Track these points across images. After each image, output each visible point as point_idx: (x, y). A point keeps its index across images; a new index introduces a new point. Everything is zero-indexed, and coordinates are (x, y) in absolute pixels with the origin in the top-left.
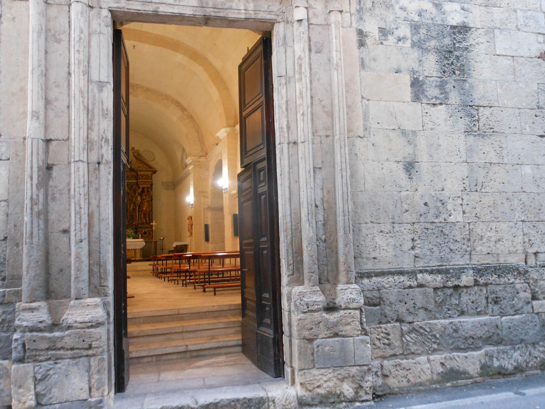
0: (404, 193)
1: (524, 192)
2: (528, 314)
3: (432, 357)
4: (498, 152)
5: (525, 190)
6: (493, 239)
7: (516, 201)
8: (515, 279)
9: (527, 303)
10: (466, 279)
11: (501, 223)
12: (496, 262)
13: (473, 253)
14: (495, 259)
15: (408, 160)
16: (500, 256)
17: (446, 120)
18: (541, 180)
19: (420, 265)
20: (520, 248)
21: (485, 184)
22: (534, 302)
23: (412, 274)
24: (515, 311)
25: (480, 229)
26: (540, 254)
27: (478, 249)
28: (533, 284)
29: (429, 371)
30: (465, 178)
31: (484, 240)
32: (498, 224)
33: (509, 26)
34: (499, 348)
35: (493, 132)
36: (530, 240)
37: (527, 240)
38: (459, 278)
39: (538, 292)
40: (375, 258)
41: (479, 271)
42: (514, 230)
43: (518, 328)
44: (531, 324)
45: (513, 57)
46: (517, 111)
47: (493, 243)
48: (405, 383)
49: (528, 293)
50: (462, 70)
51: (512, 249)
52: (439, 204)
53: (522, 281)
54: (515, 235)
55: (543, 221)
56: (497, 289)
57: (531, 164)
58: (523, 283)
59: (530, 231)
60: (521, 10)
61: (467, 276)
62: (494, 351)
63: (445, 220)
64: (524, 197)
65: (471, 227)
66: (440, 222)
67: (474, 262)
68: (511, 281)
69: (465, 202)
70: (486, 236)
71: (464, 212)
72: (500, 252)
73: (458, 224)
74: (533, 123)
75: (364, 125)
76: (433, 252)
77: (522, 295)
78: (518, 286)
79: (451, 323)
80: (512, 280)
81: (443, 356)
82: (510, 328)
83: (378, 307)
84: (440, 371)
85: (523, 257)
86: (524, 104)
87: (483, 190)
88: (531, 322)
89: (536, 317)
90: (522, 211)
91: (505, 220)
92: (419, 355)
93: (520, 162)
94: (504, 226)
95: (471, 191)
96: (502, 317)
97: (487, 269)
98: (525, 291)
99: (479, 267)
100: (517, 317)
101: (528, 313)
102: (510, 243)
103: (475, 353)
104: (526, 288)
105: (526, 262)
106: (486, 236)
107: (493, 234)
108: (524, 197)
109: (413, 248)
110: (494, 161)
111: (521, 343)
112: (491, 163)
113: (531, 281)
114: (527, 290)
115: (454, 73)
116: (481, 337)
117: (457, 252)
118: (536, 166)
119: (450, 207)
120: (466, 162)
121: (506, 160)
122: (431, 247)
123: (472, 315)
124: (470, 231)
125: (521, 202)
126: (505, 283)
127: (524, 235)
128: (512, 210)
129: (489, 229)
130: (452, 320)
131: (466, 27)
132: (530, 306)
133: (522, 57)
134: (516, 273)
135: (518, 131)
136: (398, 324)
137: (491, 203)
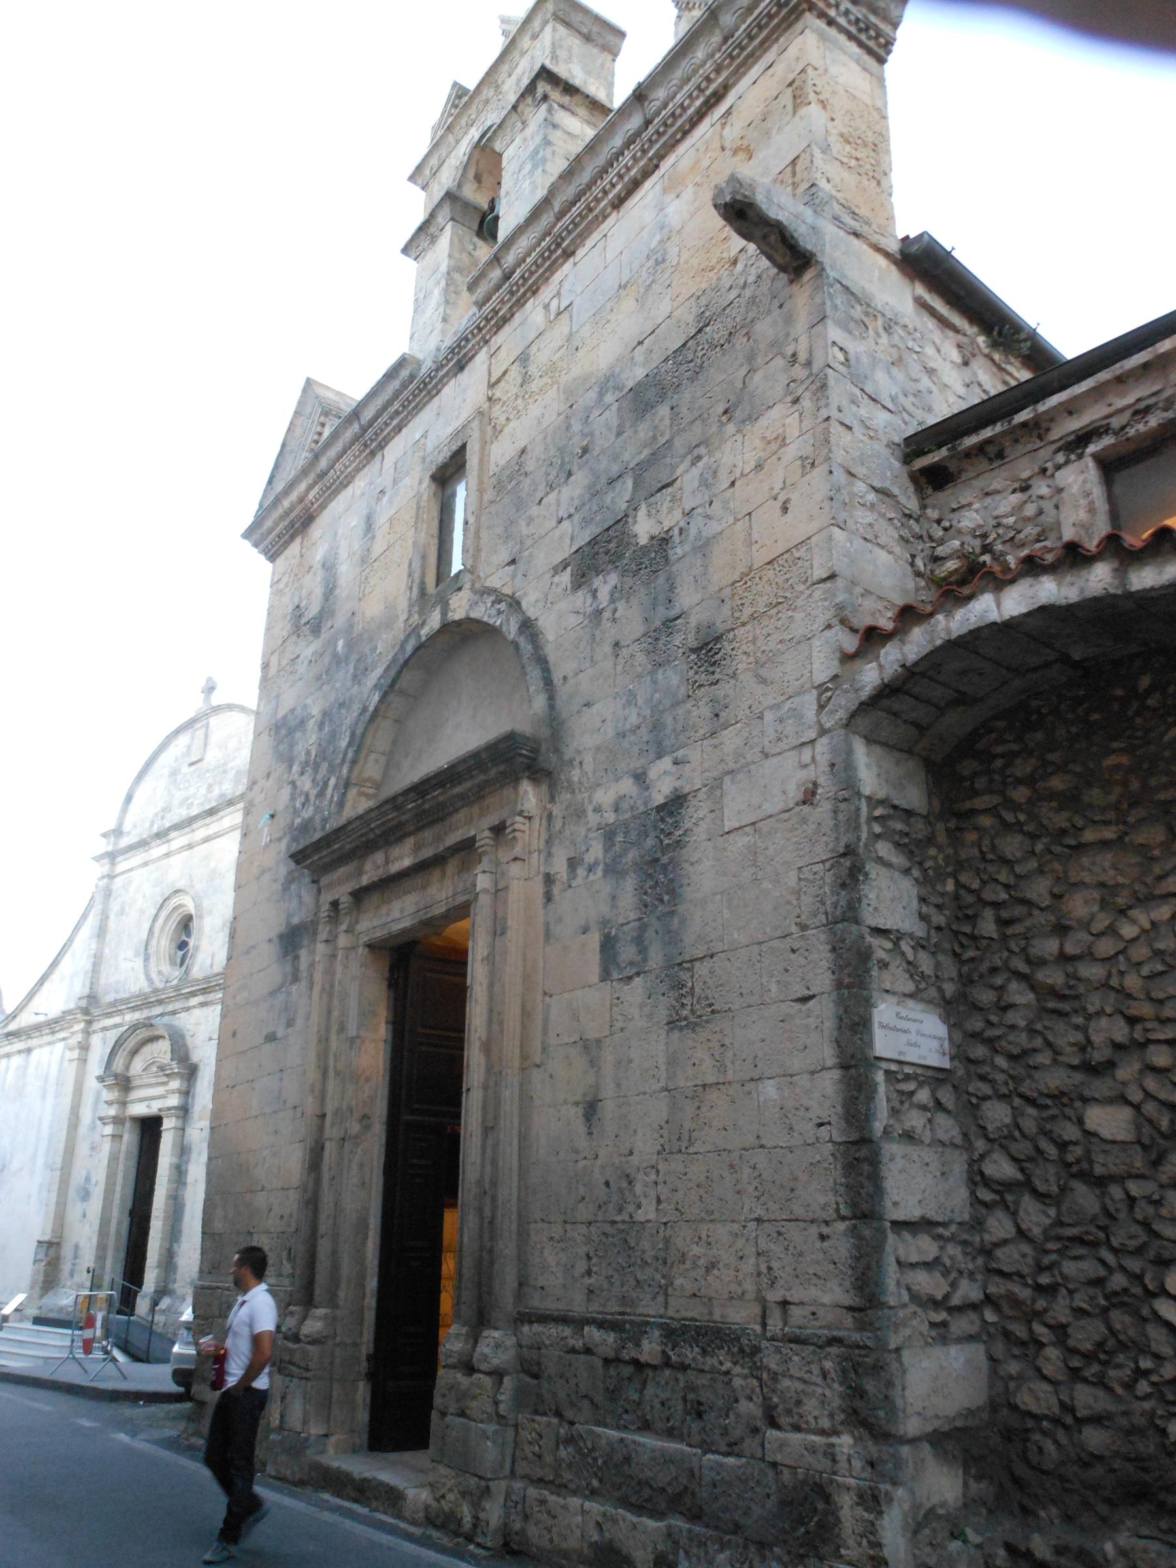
0: (581, 1164)
1: (762, 1146)
2: (752, 1461)
3: (587, 1505)
4: (717, 1057)
5: (763, 1142)
6: (702, 1262)
7: (746, 1172)
8: (735, 1364)
9: (752, 1431)
10: (650, 1348)
11: (718, 1225)
12: (707, 1318)
13: (670, 1291)
14: (706, 1311)
15: (588, 1099)
16: (715, 1302)
17: (642, 1006)
18: (798, 1113)
19: (594, 1309)
20: (749, 1286)
21: (695, 1134)
22: (772, 1434)
23: (578, 1324)
24: (730, 1445)
25: (682, 1238)
26: (792, 1307)
27: (678, 1282)
28: (769, 1383)
29: (578, 1532)
30: (663, 1124)
31: (688, 1264)
32: (711, 1226)
33: (749, 757)
34: (693, 1527)
35: (713, 1012)
36: (770, 1268)
37: (763, 1268)
38: (638, 1345)
39: (776, 1406)
40: (542, 1288)
41: (673, 1334)
42: (740, 1242)
43: (730, 1492)
44: (758, 1489)
45: (753, 824)
46: (756, 948)
47: (702, 1271)
48: (544, 1543)
49: (755, 1404)
50: (672, 892)
51: (734, 1287)
52: (624, 1184)
53: (746, 1371)
54: (740, 1254)
55: (796, 1220)
56: (699, 1382)
57: (778, 1076)
58: (746, 1377)
59: (772, 1246)
60: (771, 708)
61: (650, 1343)
62: (681, 1531)
63: (631, 1217)
64: (760, 1157)
65: (669, 1232)
66: (624, 1222)
67: (671, 1313)
68: (724, 1368)
69: (661, 1179)
70: (691, 1253)
71: (659, 1201)
72: (713, 1294)
73: (650, 1225)
74: (787, 971)
75: (542, 1043)
76: (612, 1284)
77: (744, 1407)
78: (737, 1382)
79: (622, 1440)
80: (728, 1365)
81: (602, 1509)
82: (715, 1486)
83: (535, 1382)
84: (593, 1540)
85: (757, 1310)
86: (768, 930)
87: (691, 1150)
88: (758, 1483)
89: (771, 1474)
90: (756, 1193)
91: (724, 1218)
92: (574, 1493)
93: (755, 1074)
94: (721, 1232)
95: (671, 1153)
96: (705, 1453)
97: (684, 1330)
98: (751, 1399)
99: (675, 1325)
100: (731, 1460)
101: (753, 1457)
102: (732, 1273)
103: (651, 1524)
104: (753, 1391)
105: (764, 1325)
106: (691, 1253)
107: (703, 1251)
108: (760, 1157)
109: (589, 1273)
110: (711, 1079)
111: (735, 1533)
112: (704, 1086)
113: (765, 1376)
114: (755, 1398)
115: (662, 901)
116: (663, 1490)
117: (646, 1288)
118: (788, 1079)
119: (638, 1189)
120: (666, 1090)
121: (730, 1076)
122: (610, 1272)
123: (658, 1434)
124: (667, 1241)
125: (756, 1174)
126: (713, 1370)
127: (759, 1254)
128: (738, 1192)
129: (696, 1239)
130: (624, 1435)
131: (679, 797)
132: (758, 1439)
133: (770, 816)
134: (735, 1350)
135: (754, 1000)
136: (555, 1421)
137: (702, 1178)
